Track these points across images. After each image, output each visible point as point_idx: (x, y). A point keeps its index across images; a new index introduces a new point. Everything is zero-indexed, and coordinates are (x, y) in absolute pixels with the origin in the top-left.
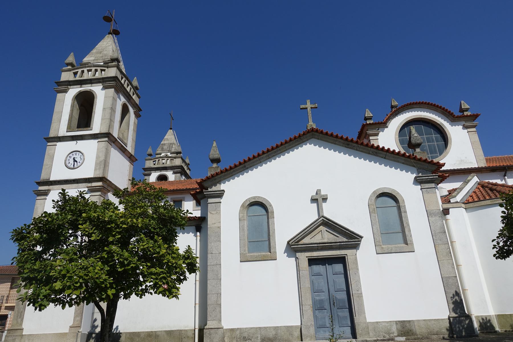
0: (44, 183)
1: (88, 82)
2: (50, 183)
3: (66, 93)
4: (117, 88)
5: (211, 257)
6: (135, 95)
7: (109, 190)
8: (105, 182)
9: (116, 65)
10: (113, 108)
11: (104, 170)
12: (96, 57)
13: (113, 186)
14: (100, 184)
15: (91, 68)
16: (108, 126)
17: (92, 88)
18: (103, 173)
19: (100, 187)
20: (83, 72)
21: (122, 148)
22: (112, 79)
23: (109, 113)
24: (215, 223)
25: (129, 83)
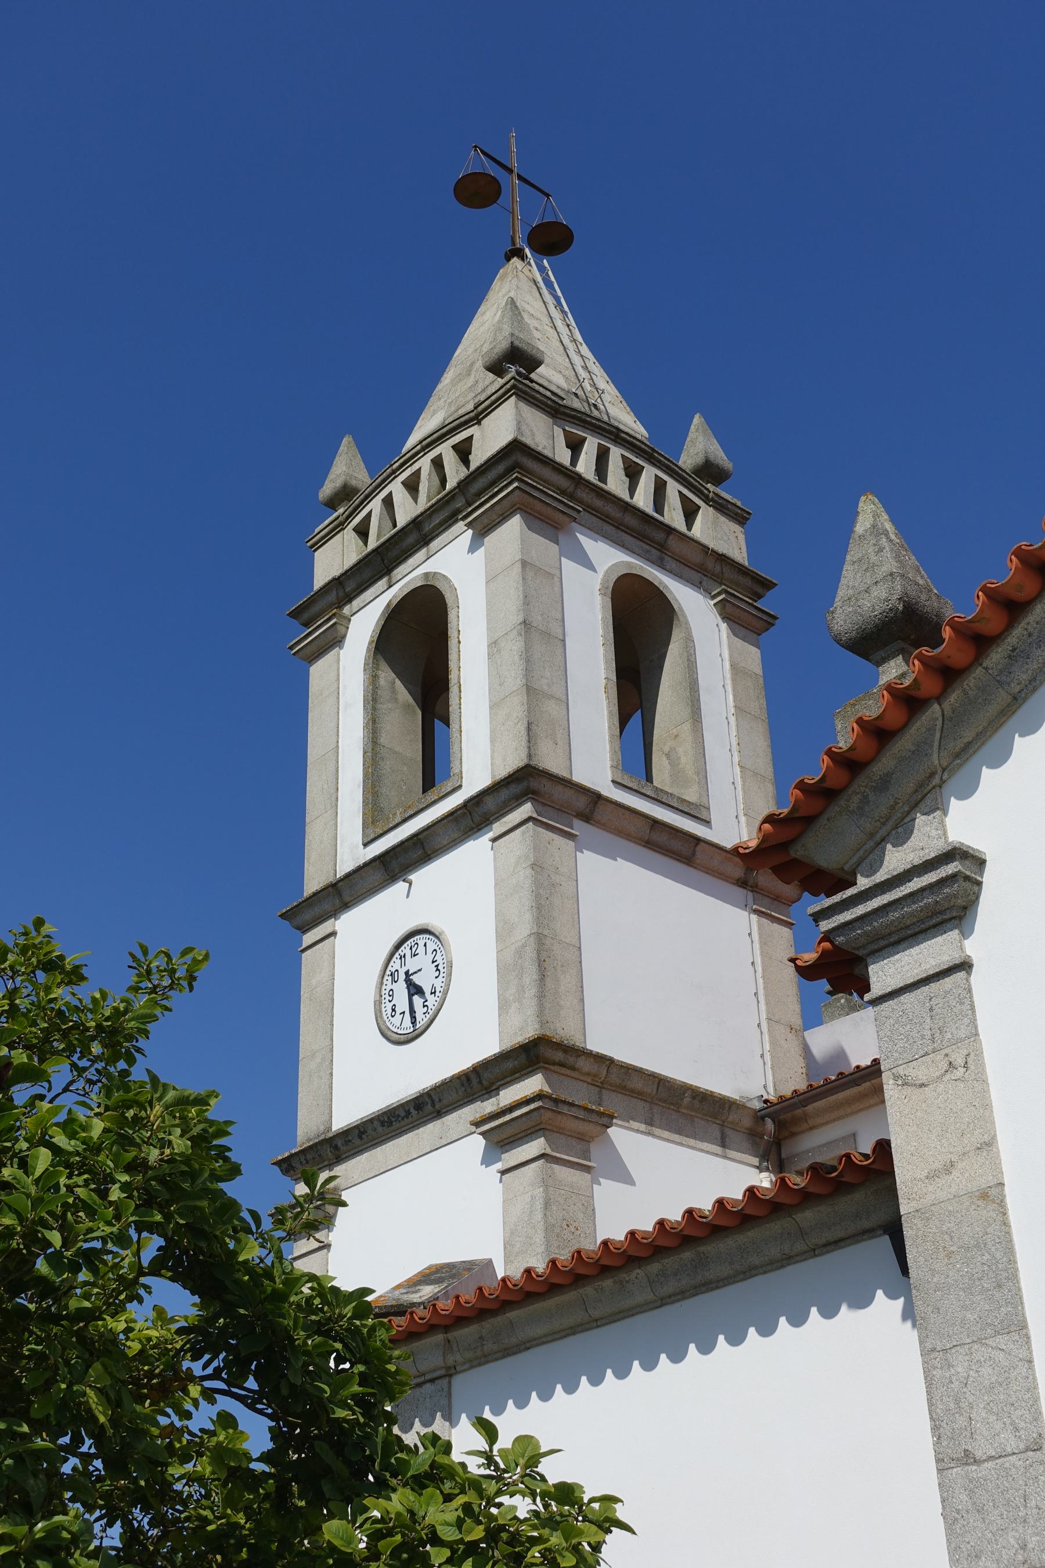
0: (309, 1157)
1: (411, 539)
2: (328, 1152)
3: (341, 648)
4: (539, 506)
5: (964, 1497)
6: (706, 515)
7: (601, 1114)
8: (562, 1065)
9: (508, 386)
10: (537, 620)
11: (541, 996)
12: (450, 404)
13: (637, 1084)
14: (533, 1084)
15: (416, 467)
16: (524, 732)
17: (428, 567)
18: (541, 1013)
19: (532, 1106)
20: (388, 502)
21: (662, 838)
22: (501, 468)
23: (517, 658)
24: (949, 1168)
25: (638, 455)
